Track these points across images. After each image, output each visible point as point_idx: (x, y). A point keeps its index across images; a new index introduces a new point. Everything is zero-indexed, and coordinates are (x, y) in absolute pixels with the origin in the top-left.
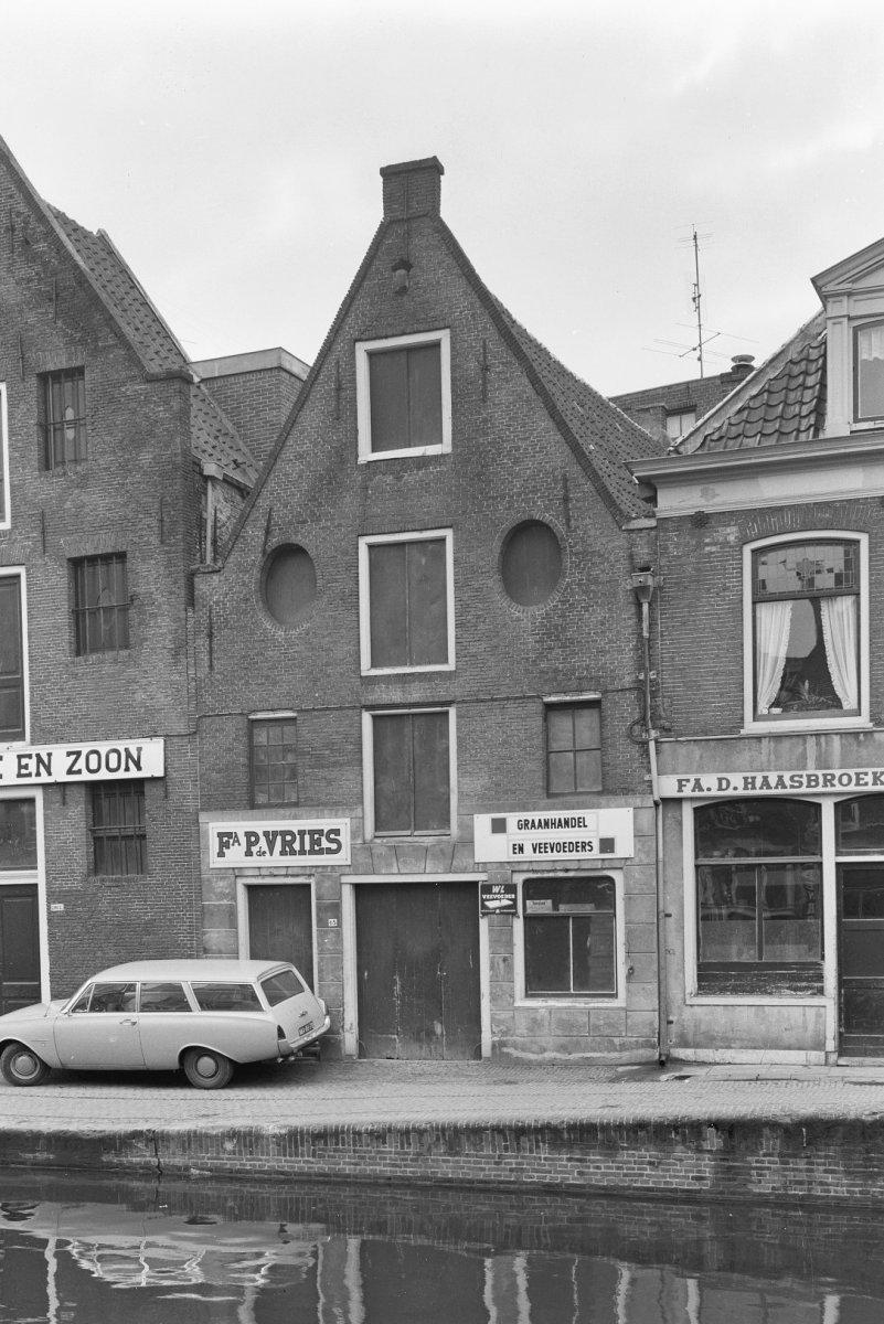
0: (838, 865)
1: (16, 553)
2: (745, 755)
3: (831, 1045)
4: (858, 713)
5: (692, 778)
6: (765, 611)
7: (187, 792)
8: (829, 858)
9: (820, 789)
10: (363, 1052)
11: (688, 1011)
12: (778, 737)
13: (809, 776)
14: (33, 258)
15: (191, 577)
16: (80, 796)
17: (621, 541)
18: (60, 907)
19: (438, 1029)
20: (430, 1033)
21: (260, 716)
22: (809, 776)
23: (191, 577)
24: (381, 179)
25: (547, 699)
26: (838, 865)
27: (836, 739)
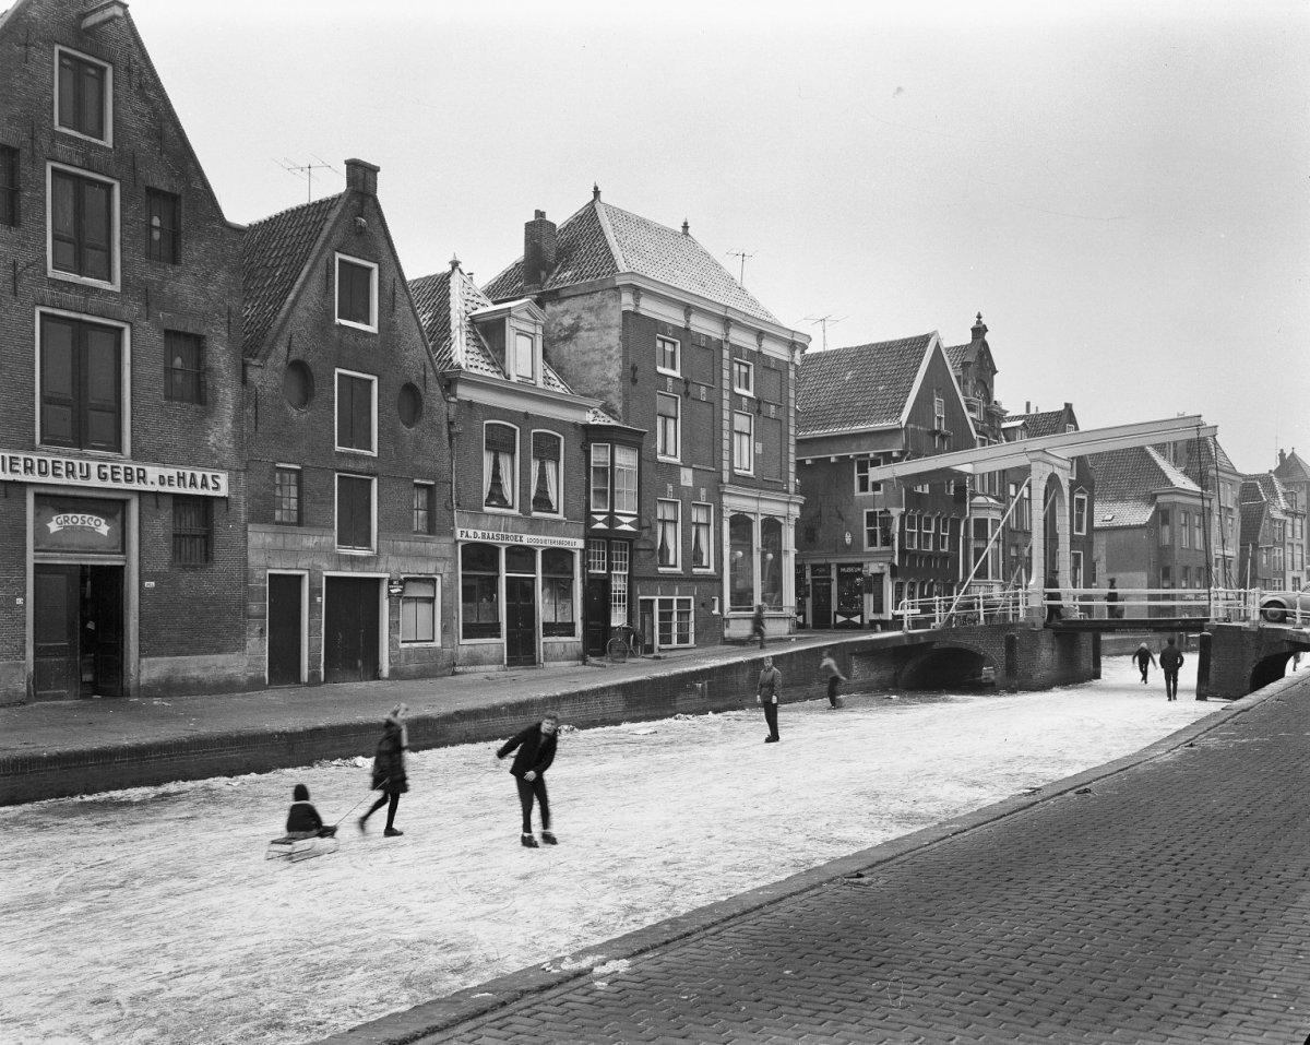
0: (507, 577)
1: (125, 312)
2: (484, 522)
3: (505, 662)
4: (675, 456)
5: (188, 473)
6: (407, 610)
7: (242, 512)
8: (504, 574)
9: (500, 541)
10: (325, 681)
11: (460, 648)
12: (495, 515)
13: (126, 468)
14: (147, 100)
15: (245, 365)
16: (169, 502)
17: (444, 405)
18: (150, 584)
19: (360, 663)
20: (356, 667)
21: (282, 465)
22: (126, 468)
23: (245, 365)
24: (513, 777)
25: (416, 481)
26: (507, 577)
27: (510, 519)
